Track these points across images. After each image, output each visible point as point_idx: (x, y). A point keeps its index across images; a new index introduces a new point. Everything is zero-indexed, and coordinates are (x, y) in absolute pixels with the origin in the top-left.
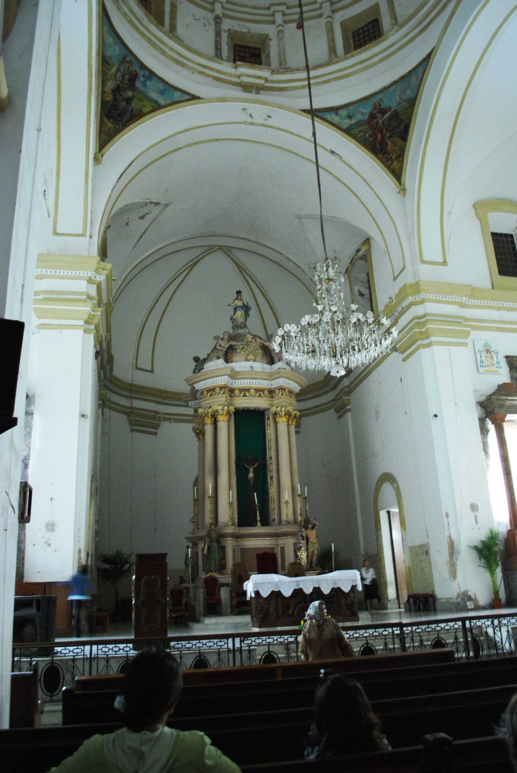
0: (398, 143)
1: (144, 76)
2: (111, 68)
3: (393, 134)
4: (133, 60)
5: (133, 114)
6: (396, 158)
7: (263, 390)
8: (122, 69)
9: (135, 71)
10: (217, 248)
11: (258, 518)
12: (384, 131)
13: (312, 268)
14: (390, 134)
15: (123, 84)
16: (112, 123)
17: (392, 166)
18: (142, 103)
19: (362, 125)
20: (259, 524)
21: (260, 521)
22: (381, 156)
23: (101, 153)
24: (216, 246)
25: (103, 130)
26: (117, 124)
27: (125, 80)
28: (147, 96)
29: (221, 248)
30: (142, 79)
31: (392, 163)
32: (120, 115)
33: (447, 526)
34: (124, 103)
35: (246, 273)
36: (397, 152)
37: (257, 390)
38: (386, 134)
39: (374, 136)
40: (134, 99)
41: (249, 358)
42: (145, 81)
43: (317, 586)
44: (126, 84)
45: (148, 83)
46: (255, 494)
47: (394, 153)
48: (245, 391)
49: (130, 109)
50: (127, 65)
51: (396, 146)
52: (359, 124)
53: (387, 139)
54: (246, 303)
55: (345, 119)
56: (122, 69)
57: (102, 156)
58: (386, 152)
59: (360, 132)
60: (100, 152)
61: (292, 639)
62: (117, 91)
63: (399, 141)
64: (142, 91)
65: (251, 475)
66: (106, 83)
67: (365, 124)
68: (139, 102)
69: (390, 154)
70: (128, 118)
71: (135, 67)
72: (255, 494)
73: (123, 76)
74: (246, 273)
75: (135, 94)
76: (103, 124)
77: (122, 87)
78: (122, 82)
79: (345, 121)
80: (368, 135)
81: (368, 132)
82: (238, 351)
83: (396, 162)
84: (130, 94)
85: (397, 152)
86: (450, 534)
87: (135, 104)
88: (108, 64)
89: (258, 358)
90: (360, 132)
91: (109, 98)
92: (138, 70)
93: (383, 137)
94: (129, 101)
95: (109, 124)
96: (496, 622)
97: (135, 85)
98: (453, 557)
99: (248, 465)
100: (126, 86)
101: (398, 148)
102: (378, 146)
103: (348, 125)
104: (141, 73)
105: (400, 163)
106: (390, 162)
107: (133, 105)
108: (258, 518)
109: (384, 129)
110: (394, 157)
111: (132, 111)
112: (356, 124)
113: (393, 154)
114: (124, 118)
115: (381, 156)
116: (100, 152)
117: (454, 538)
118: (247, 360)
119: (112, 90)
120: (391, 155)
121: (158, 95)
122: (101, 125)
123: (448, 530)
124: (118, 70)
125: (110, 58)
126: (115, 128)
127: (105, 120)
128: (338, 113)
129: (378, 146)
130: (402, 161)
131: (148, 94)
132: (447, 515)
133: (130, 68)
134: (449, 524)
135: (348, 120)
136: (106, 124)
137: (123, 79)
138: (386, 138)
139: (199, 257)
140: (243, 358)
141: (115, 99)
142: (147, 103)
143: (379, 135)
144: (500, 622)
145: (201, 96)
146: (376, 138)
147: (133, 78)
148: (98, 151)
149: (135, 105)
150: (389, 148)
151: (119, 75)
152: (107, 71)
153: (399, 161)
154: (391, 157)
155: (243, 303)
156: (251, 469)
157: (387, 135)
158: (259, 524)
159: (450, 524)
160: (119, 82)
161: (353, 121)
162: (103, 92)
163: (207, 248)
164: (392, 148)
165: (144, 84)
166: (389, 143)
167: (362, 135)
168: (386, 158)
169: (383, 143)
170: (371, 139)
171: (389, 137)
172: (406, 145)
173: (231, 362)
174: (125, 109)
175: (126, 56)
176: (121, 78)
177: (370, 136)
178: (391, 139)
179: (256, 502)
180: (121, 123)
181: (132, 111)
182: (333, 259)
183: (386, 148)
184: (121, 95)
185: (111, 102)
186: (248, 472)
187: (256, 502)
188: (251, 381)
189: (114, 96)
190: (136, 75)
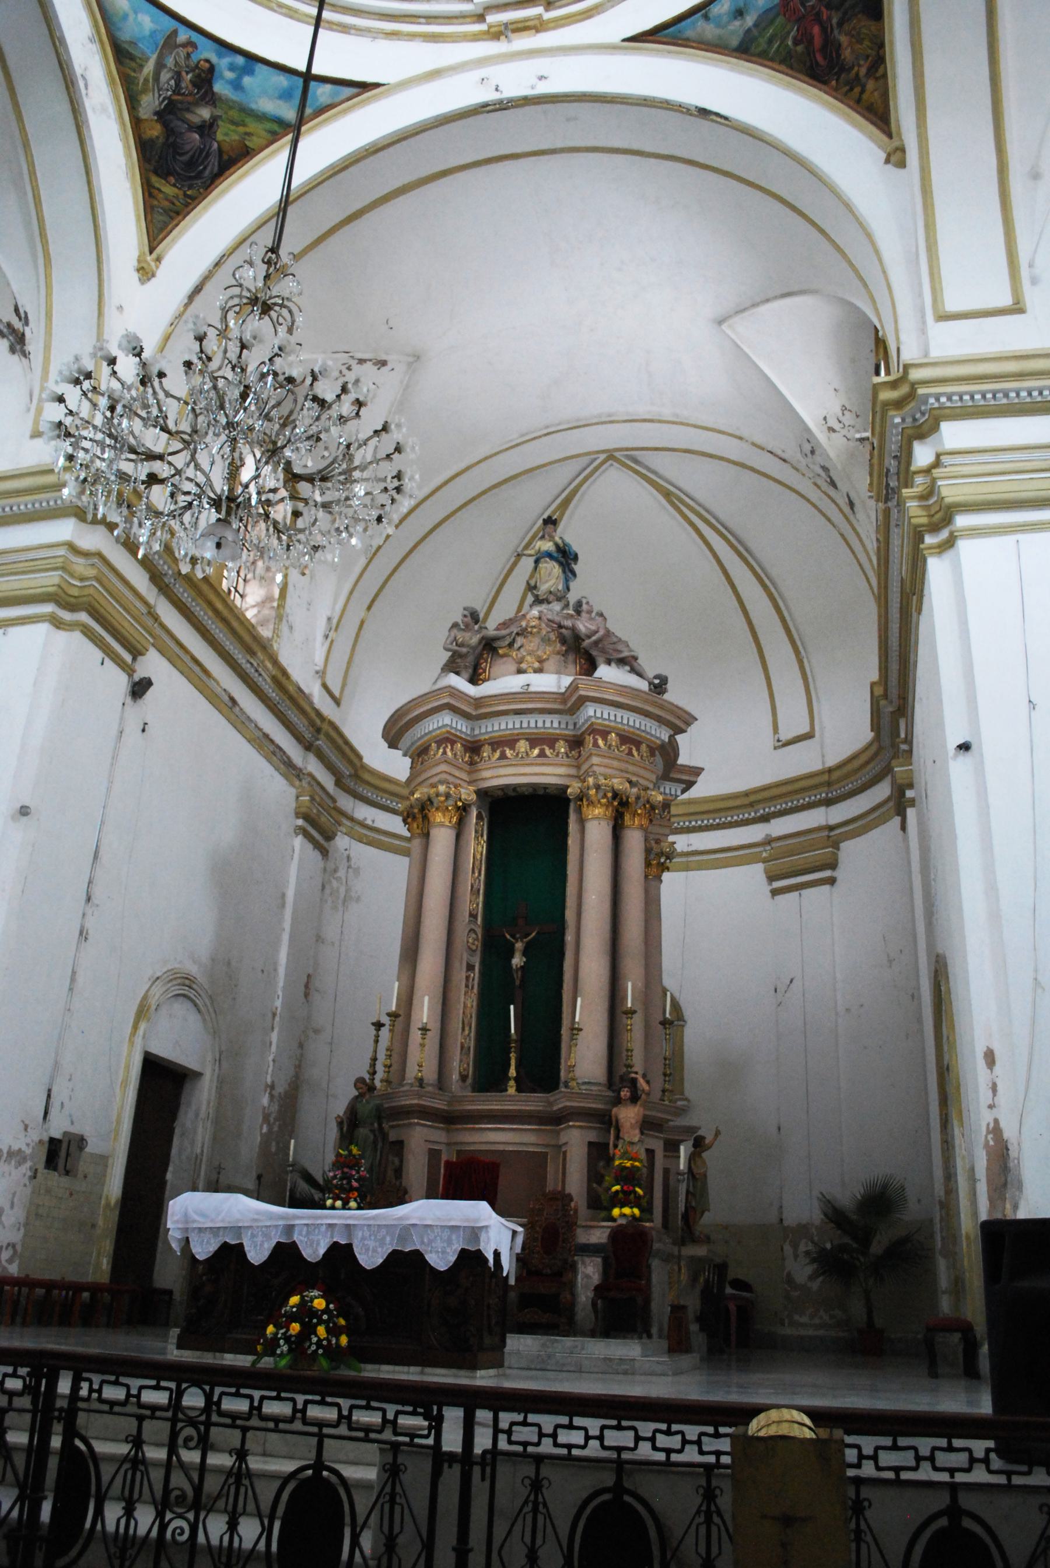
0: (864, 31)
1: (232, 68)
2: (141, 66)
3: (845, 13)
4: (195, 37)
5: (225, 157)
6: (869, 70)
7: (551, 741)
8: (170, 61)
9: (207, 61)
10: (603, 457)
11: (512, 1072)
12: (825, 14)
13: (809, 455)
14: (840, 14)
15: (179, 94)
16: (174, 185)
17: (865, 96)
18: (241, 129)
19: (772, 22)
20: (512, 1090)
21: (516, 1079)
22: (834, 83)
23: (154, 255)
24: (598, 452)
25: (155, 203)
26: (190, 187)
27: (183, 85)
28: (252, 110)
29: (611, 456)
30: (229, 75)
31: (863, 92)
32: (191, 164)
33: (990, 1093)
34: (197, 136)
35: (688, 506)
36: (868, 57)
37: (534, 741)
38: (830, 19)
39: (806, 37)
40: (220, 123)
41: (524, 666)
42: (239, 78)
43: (343, 1242)
44: (191, 94)
45: (247, 80)
46: (512, 1007)
47: (862, 62)
48: (503, 743)
49: (215, 145)
50: (182, 52)
51: (860, 41)
52: (765, 20)
53: (836, 32)
54: (560, 542)
55: (729, 22)
56: (170, 61)
57: (159, 260)
58: (843, 69)
59: (770, 42)
60: (151, 252)
61: (160, 1398)
62: (168, 113)
63: (864, 25)
64: (234, 102)
65: (517, 961)
66: (139, 101)
67: (778, 15)
68: (233, 127)
69: (852, 68)
70: (216, 169)
71: (206, 52)
72: (512, 1007)
73: (178, 76)
74: (688, 506)
75: (218, 112)
76: (153, 190)
77: (181, 102)
78: (177, 90)
79: (731, 27)
80: (790, 43)
81: (789, 33)
82: (501, 651)
83: (871, 85)
84: (205, 113)
85: (868, 57)
86: (996, 1121)
87: (226, 134)
88: (132, 58)
89: (550, 665)
90: (770, 42)
91: (155, 131)
92: (214, 59)
93: (824, 30)
94: (207, 129)
95: (169, 190)
96: (193, 1399)
97: (213, 93)
98: (1004, 1199)
99: (513, 936)
100: (190, 99)
101: (867, 43)
102: (819, 58)
103: (741, 33)
104: (223, 63)
105: (881, 81)
106: (857, 90)
107: (220, 136)
108: (512, 1072)
109: (823, 9)
110: (863, 71)
111: (220, 151)
112: (756, 25)
113: (859, 66)
114: (205, 168)
115: (834, 83)
116: (151, 252)
117: (1009, 1132)
118: (520, 671)
119: (156, 113)
120: (856, 69)
121: (280, 102)
122: (149, 192)
123: (991, 1107)
124: (160, 66)
125: (133, 43)
126: (185, 195)
127: (155, 180)
128: (711, 15)
129: (819, 58)
130: (885, 76)
131: (253, 106)
132: (990, 1058)
133: (192, 56)
134: (994, 1088)
135: (737, 23)
136: (159, 190)
137: (177, 84)
138: (832, 30)
139: (572, 486)
140: (513, 667)
141: (169, 130)
142: (253, 126)
143: (816, 30)
144: (212, 1405)
145: (381, 81)
146: (810, 41)
147: (205, 76)
148: (147, 249)
149: (226, 135)
150: (847, 54)
151: (165, 76)
152: (133, 74)
153: (877, 79)
154: (857, 74)
155: (557, 545)
156: (519, 945)
157: (834, 21)
158: (512, 1090)
159: (1000, 1088)
160: (169, 93)
161: (750, 20)
162: (136, 123)
163: (586, 460)
164: (853, 51)
165: (237, 85)
166: (844, 39)
167: (779, 46)
168: (847, 83)
169: (830, 47)
170: (800, 48)
171: (840, 24)
172: (882, 30)
173: (484, 681)
174: (201, 151)
175: (175, 32)
176: (172, 82)
177: (796, 42)
178: (846, 27)
179: (513, 1031)
180: (199, 182)
181: (220, 151)
182: (840, 414)
183: (839, 56)
184: (184, 121)
185: (161, 140)
186: (511, 954)
187: (513, 1031)
188: (517, 719)
189: (166, 125)
190: (212, 69)
